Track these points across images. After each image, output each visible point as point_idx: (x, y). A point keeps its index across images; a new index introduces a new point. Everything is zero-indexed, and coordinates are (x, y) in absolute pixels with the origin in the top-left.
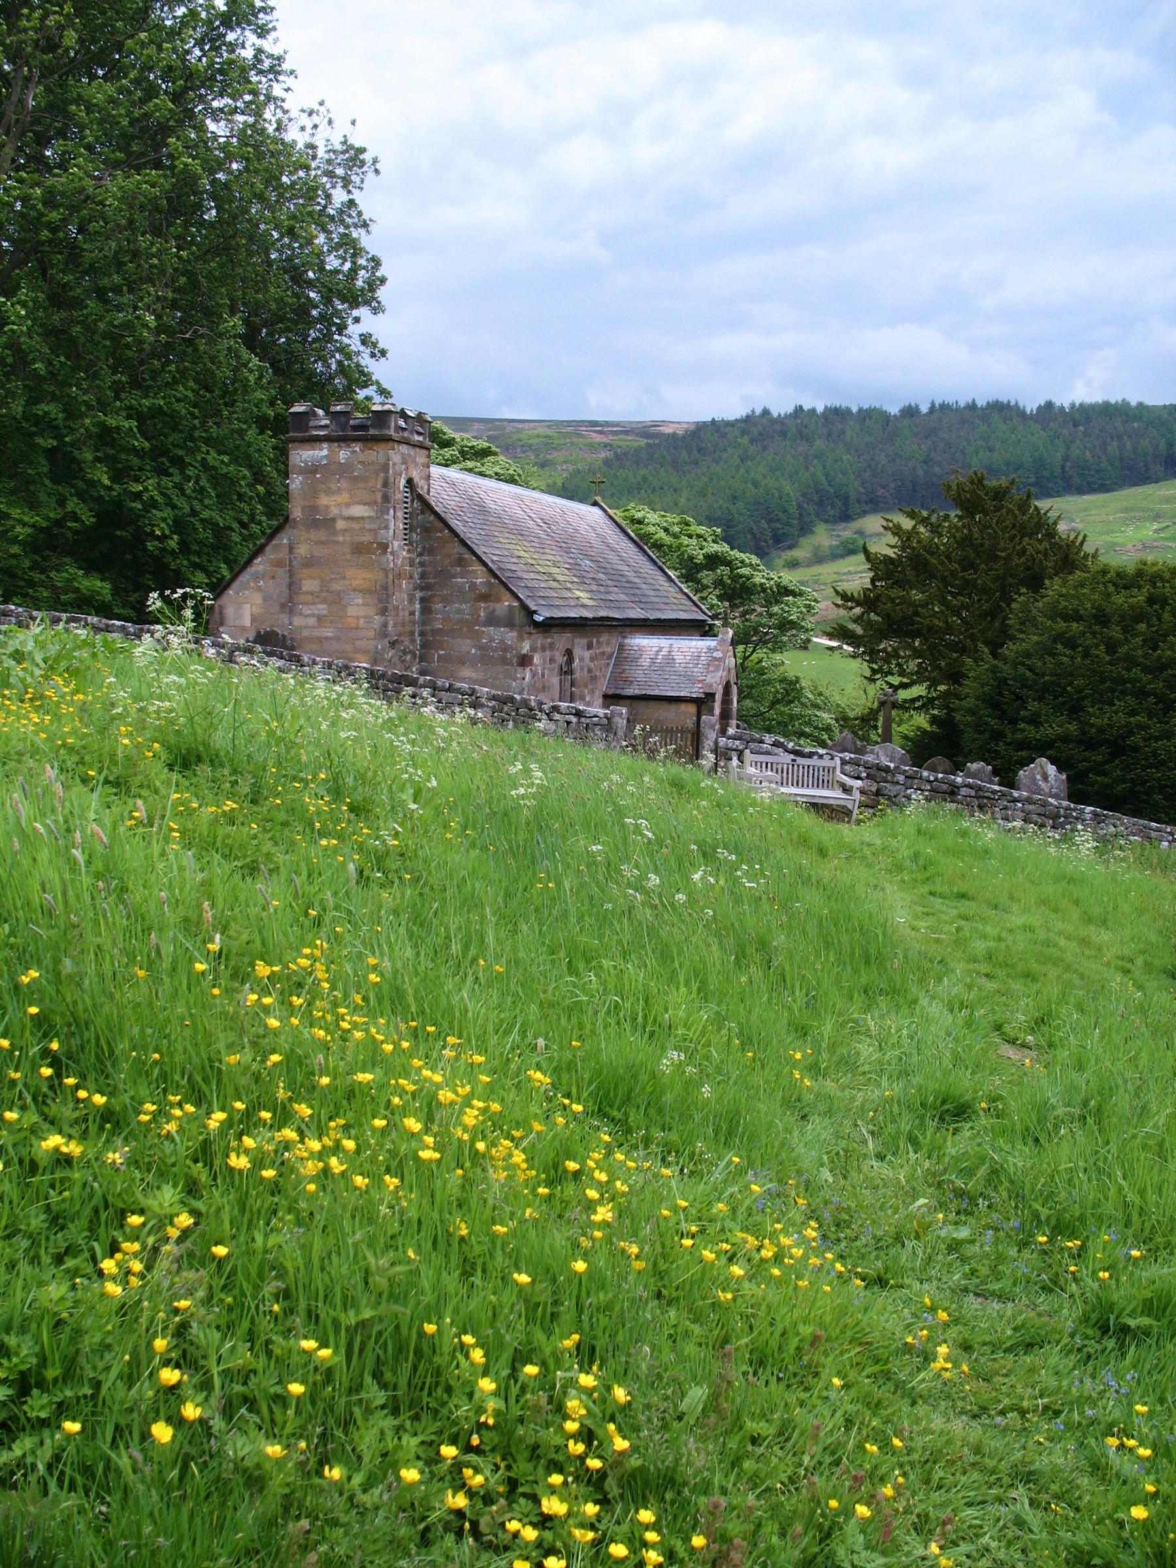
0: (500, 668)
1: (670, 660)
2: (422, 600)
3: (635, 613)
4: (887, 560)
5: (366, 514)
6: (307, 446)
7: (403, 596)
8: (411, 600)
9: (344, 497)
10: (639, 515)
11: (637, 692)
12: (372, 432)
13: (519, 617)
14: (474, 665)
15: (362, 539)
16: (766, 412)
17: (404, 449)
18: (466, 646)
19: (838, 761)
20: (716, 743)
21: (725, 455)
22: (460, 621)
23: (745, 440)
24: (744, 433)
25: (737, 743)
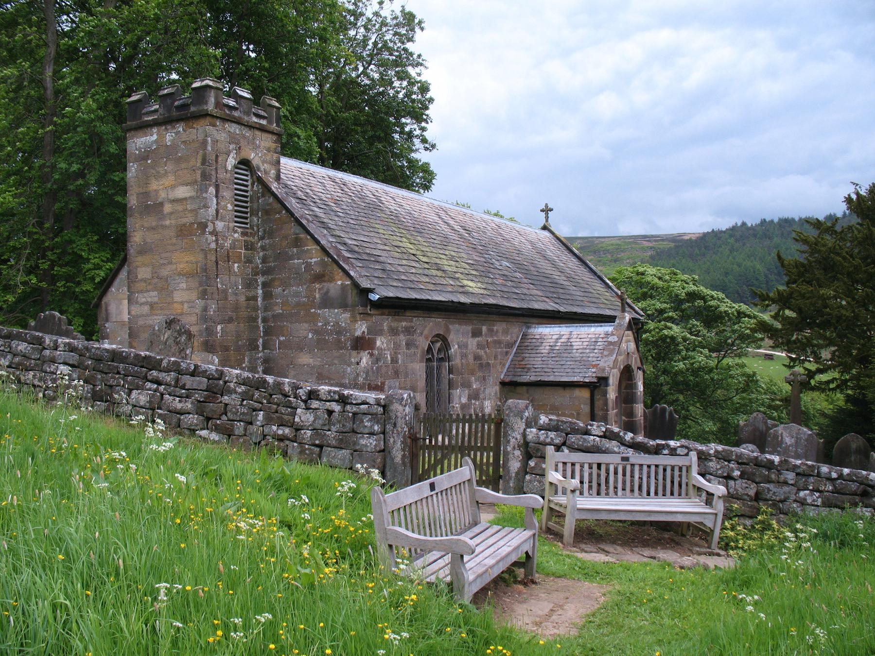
0: (335, 353)
1: (568, 346)
2: (265, 285)
3: (551, 306)
4: (797, 265)
5: (188, 195)
6: (140, 133)
7: (232, 280)
8: (249, 284)
9: (170, 180)
10: (641, 269)
11: (533, 379)
12: (193, 109)
13: (352, 297)
14: (310, 351)
15: (185, 220)
16: (744, 224)
17: (234, 128)
18: (303, 331)
19: (693, 456)
20: (524, 435)
21: (720, 250)
22: (298, 304)
23: (732, 240)
24: (731, 236)
25: (552, 435)
